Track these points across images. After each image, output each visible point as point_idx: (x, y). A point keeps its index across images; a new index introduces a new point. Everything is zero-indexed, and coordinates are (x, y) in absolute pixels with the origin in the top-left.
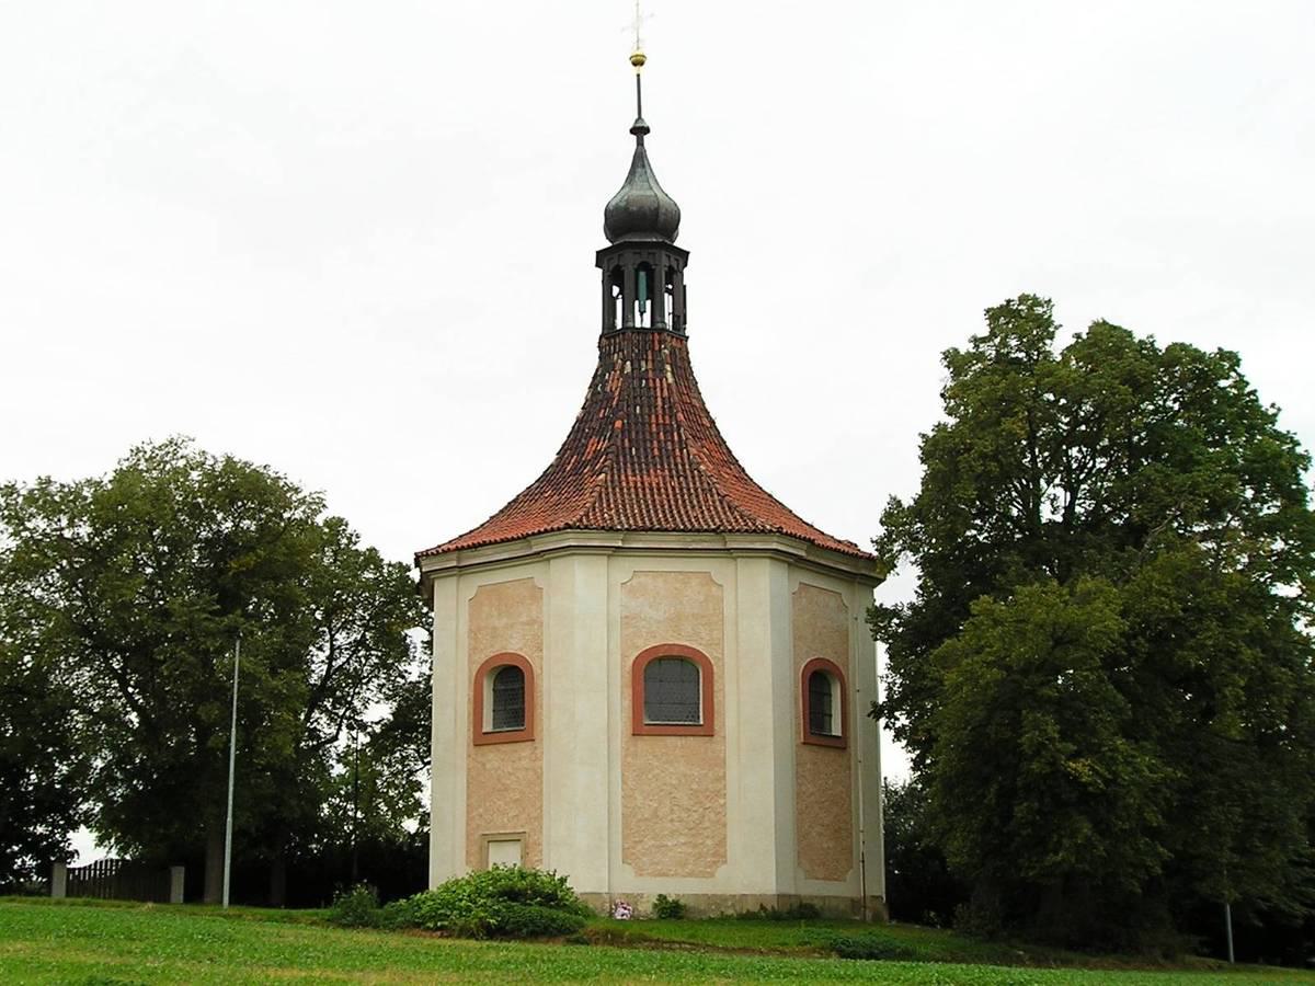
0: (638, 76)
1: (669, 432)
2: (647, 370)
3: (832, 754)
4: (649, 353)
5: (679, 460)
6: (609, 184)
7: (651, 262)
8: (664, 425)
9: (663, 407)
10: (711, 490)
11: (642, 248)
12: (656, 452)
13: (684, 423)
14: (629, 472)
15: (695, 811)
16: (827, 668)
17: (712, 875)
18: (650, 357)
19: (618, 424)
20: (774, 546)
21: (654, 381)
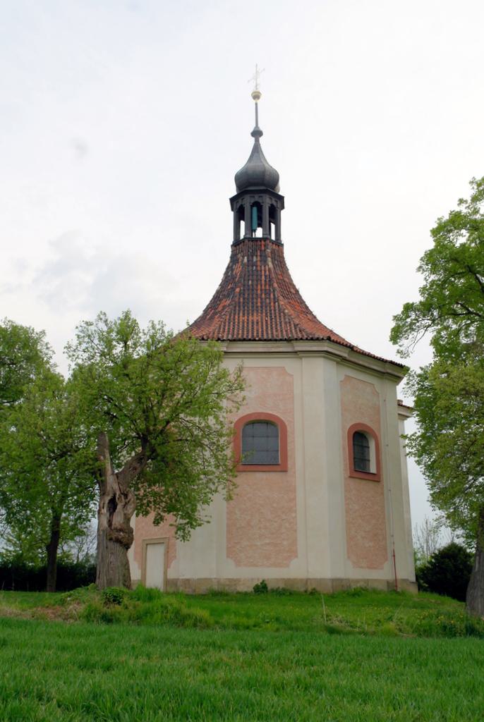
0: (256, 104)
1: (268, 293)
2: (257, 261)
3: (371, 485)
4: (259, 252)
5: (272, 308)
6: (239, 161)
7: (260, 201)
8: (266, 290)
9: (265, 281)
10: (290, 323)
11: (257, 197)
12: (259, 304)
13: (278, 289)
14: (241, 314)
15: (276, 522)
16: (367, 430)
17: (287, 566)
18: (259, 254)
19: (238, 290)
20: (325, 349)
21: (261, 267)
